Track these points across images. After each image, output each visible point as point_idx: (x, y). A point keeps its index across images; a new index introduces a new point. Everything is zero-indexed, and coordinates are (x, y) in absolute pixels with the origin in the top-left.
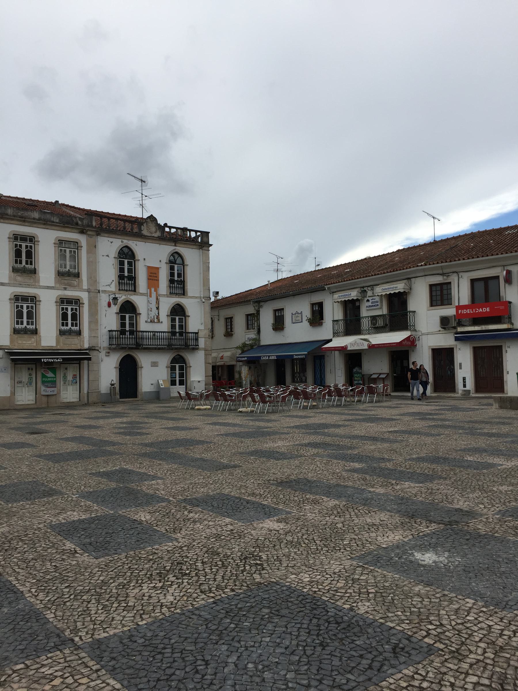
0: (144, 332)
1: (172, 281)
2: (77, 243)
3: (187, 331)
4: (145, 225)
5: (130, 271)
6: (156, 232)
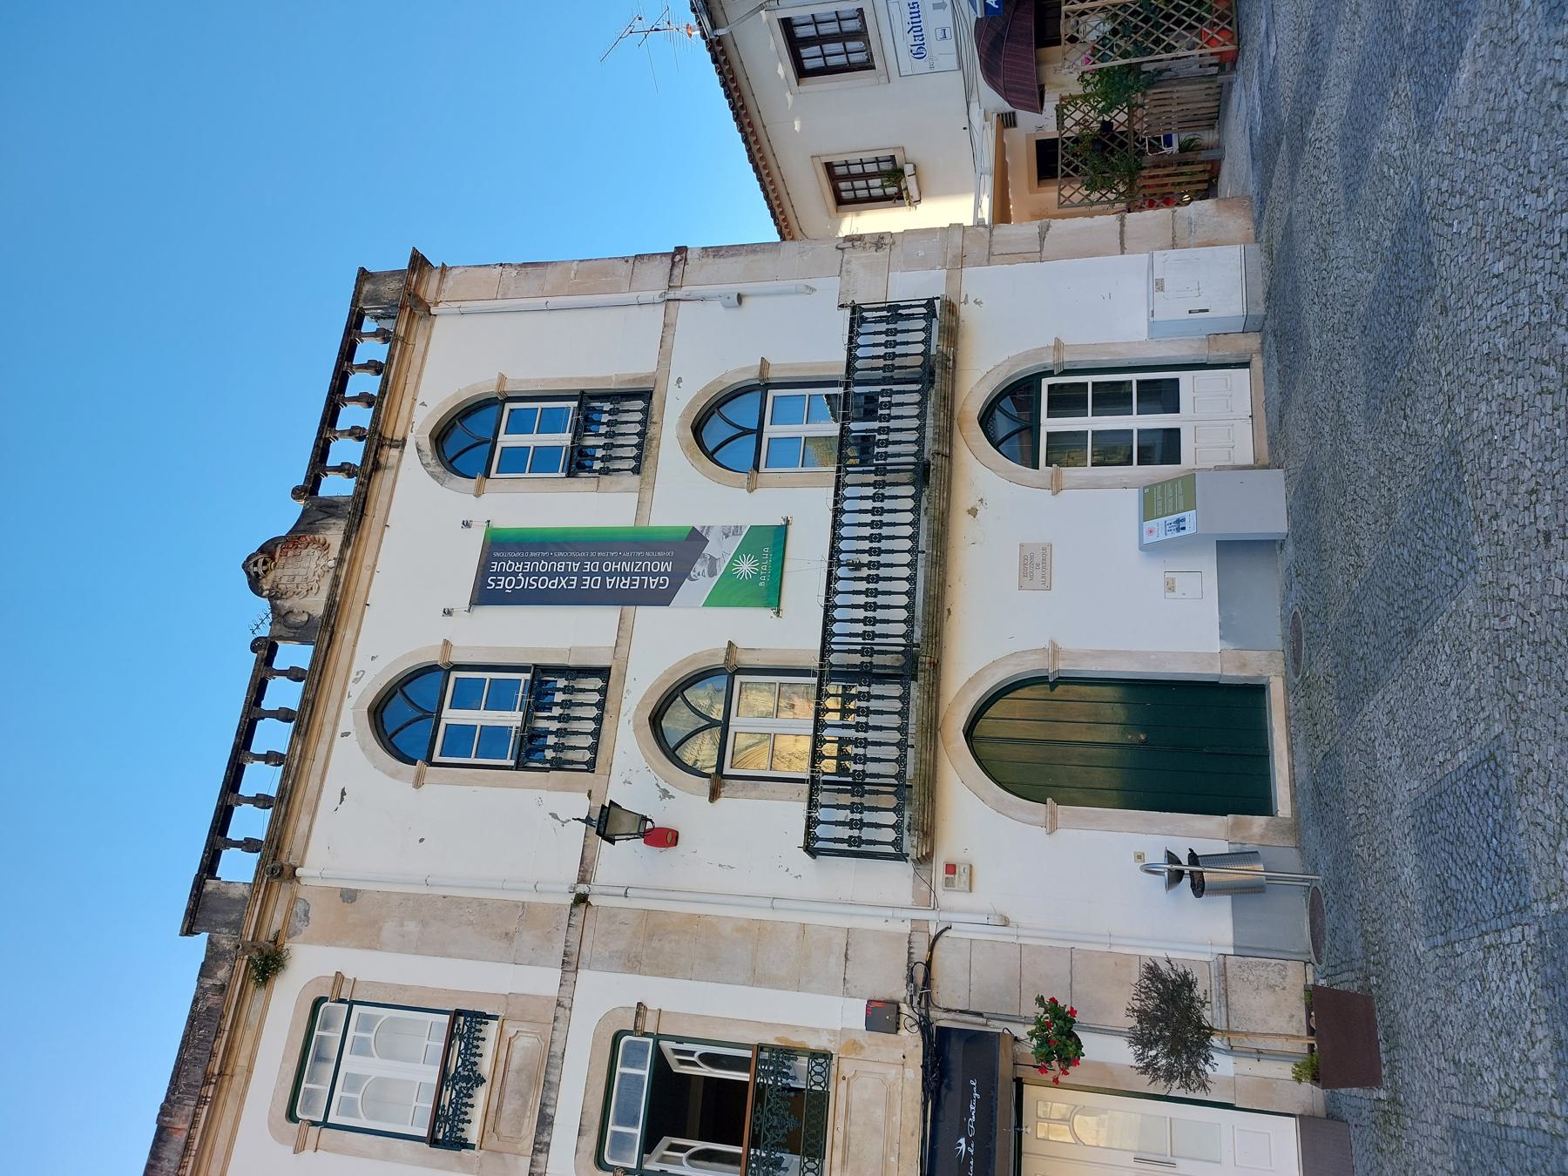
0: (827, 634)
1: (578, 463)
2: (318, 1003)
3: (840, 372)
4: (286, 604)
5: (550, 423)
6: (325, 546)
